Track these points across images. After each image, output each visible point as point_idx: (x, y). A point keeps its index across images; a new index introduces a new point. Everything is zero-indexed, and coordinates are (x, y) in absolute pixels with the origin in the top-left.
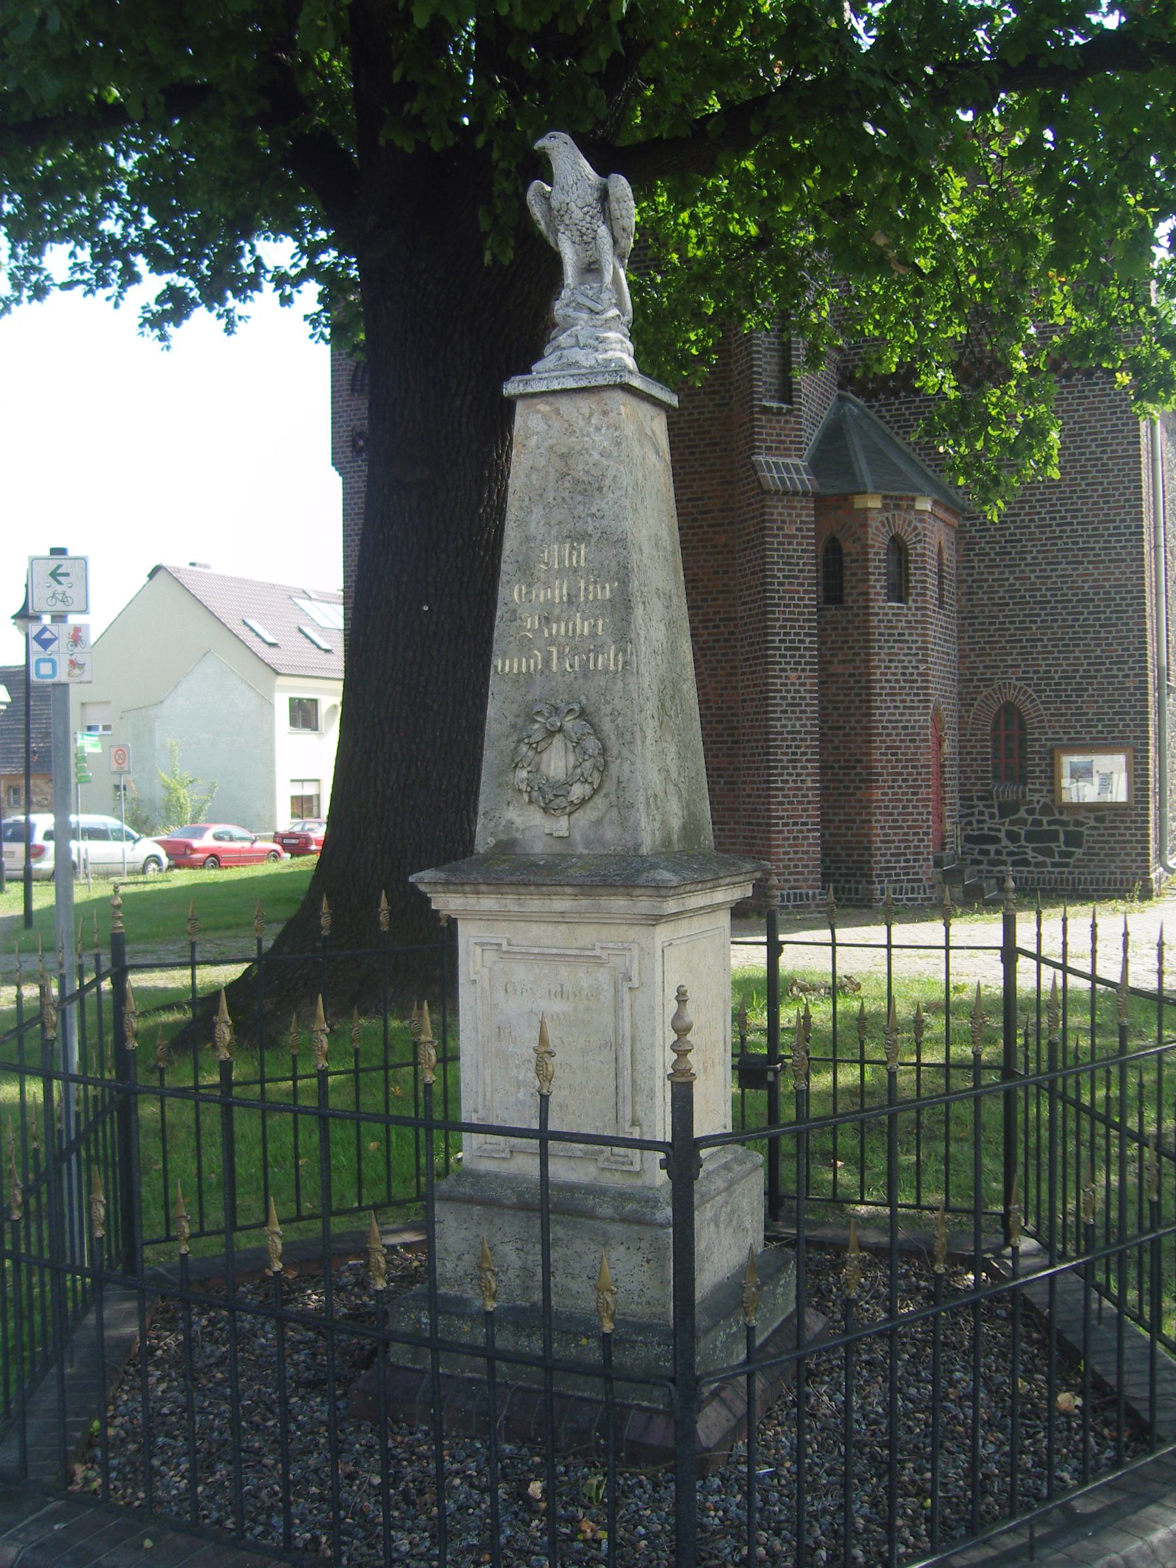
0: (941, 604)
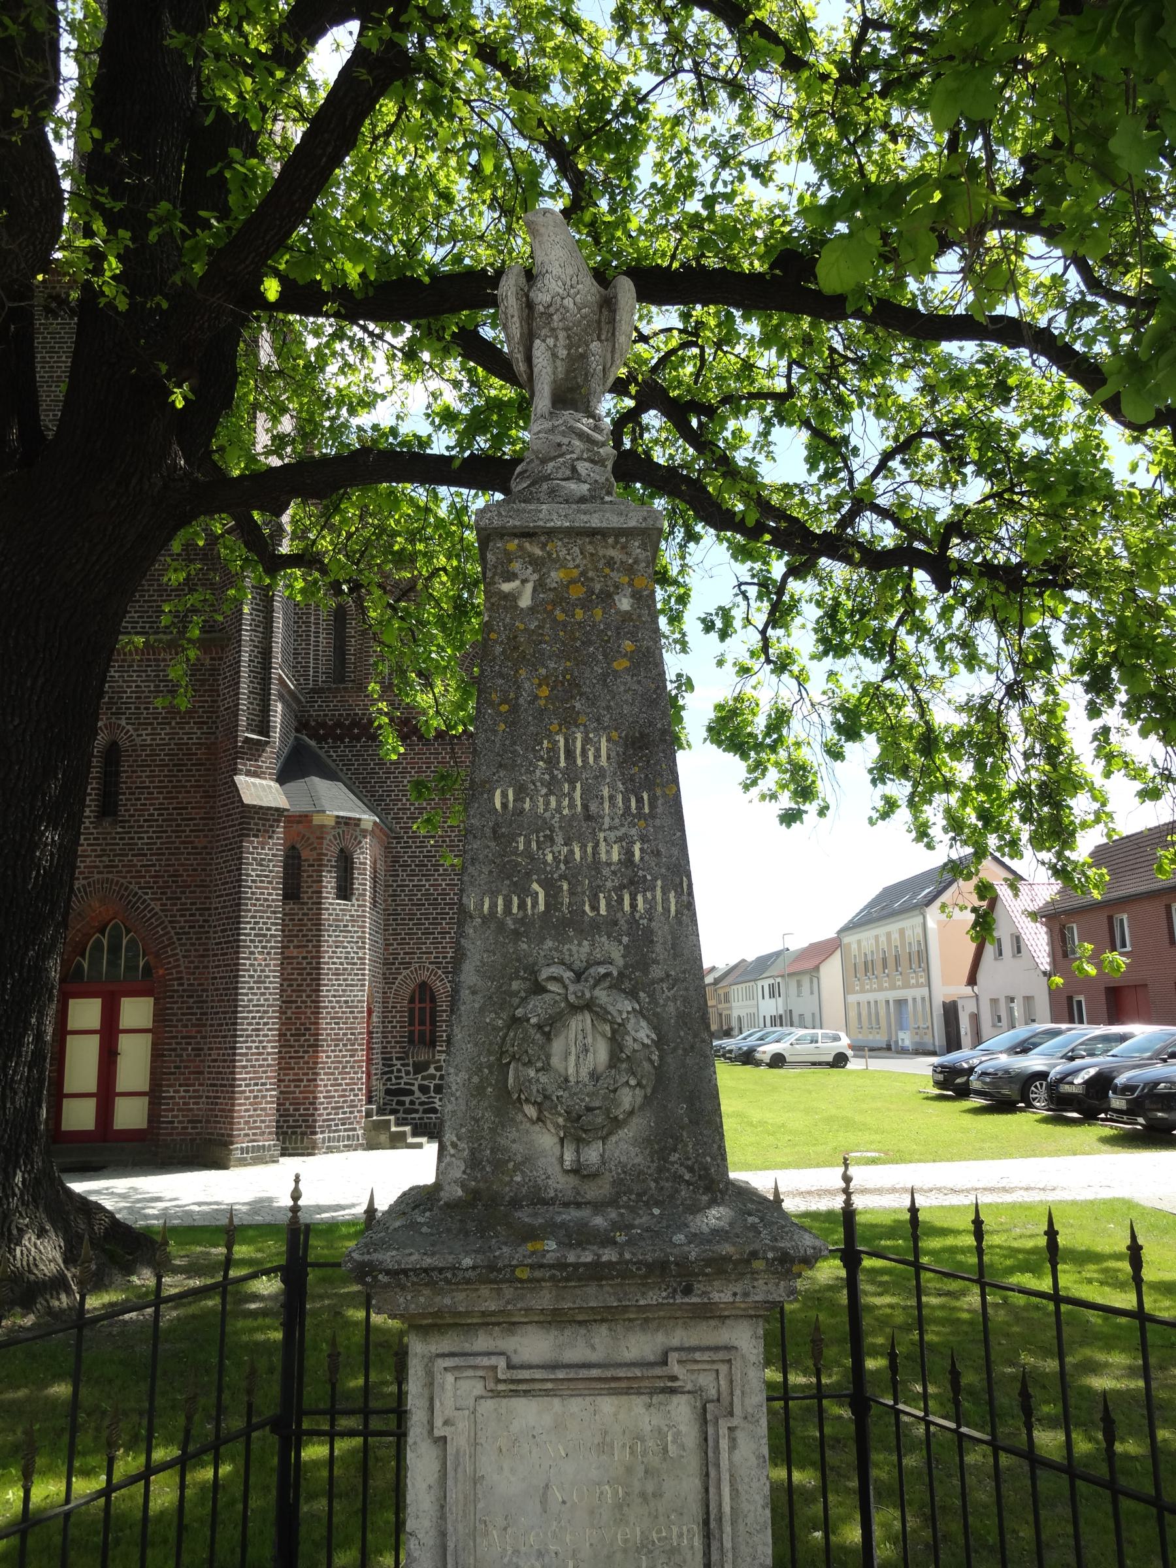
0: (374, 903)
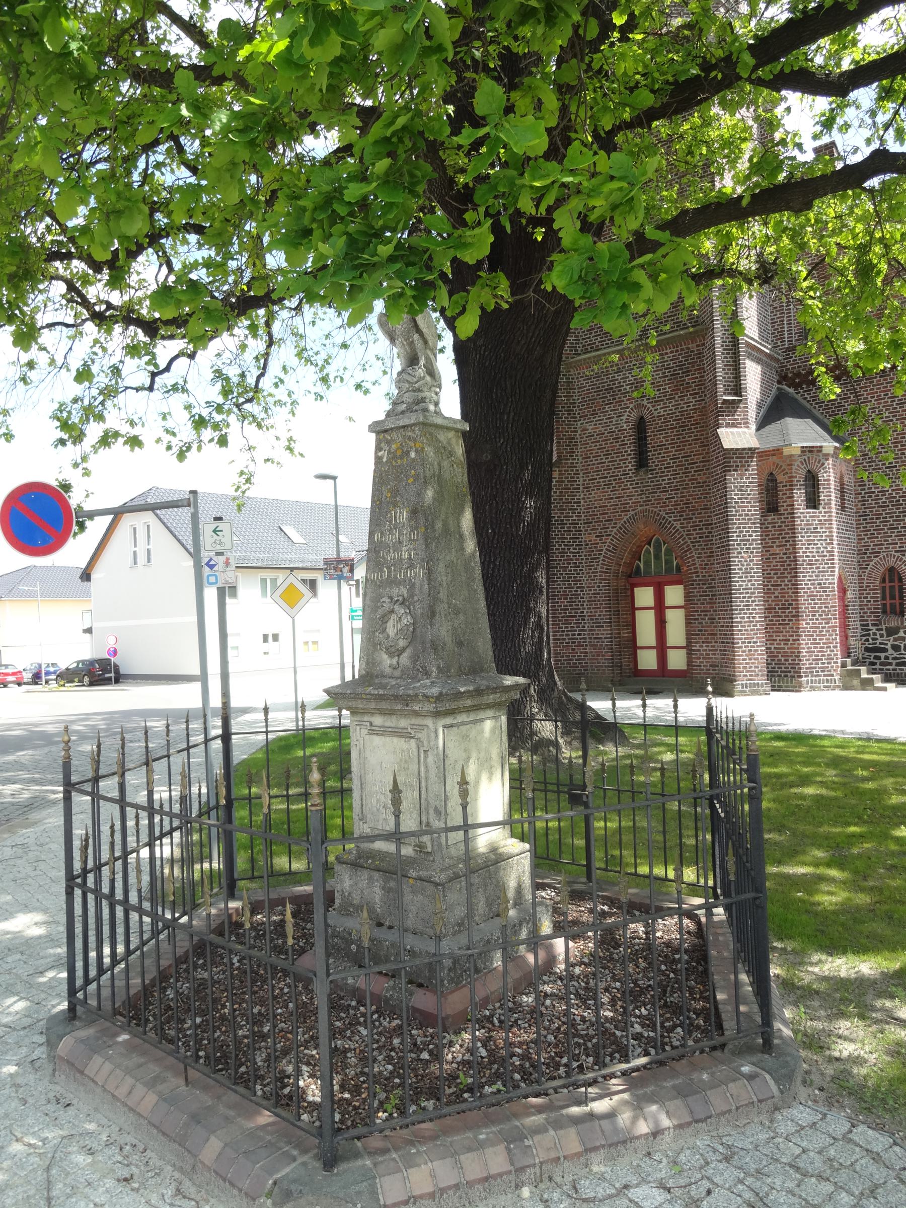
0: (843, 508)
